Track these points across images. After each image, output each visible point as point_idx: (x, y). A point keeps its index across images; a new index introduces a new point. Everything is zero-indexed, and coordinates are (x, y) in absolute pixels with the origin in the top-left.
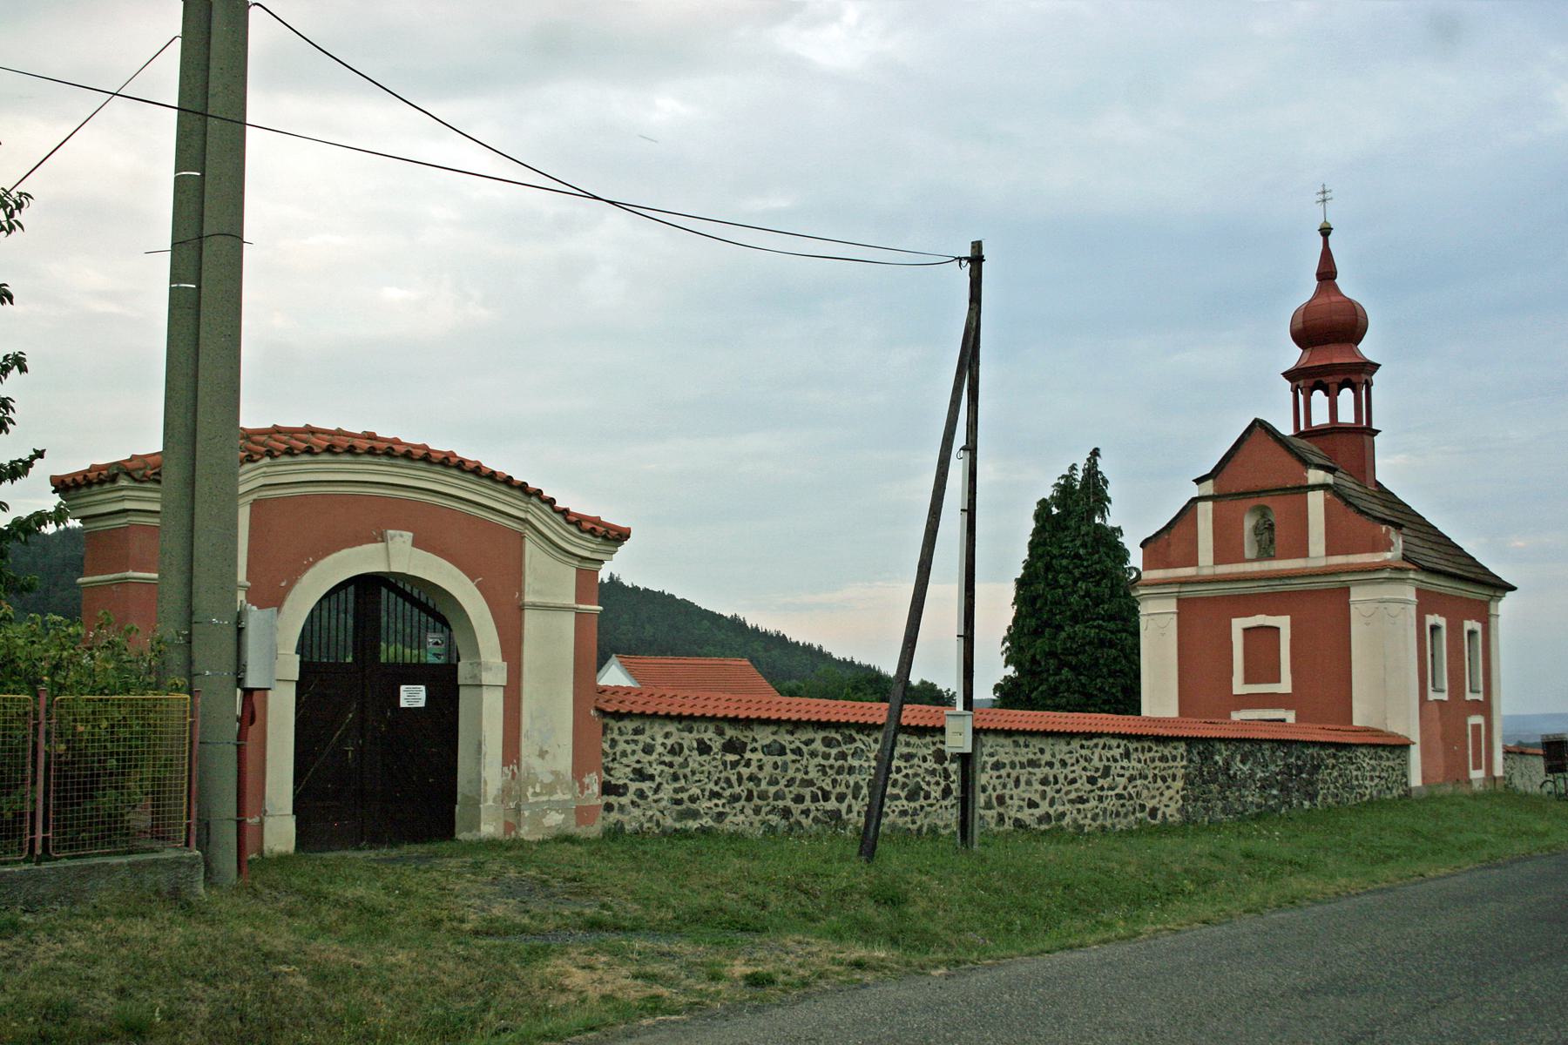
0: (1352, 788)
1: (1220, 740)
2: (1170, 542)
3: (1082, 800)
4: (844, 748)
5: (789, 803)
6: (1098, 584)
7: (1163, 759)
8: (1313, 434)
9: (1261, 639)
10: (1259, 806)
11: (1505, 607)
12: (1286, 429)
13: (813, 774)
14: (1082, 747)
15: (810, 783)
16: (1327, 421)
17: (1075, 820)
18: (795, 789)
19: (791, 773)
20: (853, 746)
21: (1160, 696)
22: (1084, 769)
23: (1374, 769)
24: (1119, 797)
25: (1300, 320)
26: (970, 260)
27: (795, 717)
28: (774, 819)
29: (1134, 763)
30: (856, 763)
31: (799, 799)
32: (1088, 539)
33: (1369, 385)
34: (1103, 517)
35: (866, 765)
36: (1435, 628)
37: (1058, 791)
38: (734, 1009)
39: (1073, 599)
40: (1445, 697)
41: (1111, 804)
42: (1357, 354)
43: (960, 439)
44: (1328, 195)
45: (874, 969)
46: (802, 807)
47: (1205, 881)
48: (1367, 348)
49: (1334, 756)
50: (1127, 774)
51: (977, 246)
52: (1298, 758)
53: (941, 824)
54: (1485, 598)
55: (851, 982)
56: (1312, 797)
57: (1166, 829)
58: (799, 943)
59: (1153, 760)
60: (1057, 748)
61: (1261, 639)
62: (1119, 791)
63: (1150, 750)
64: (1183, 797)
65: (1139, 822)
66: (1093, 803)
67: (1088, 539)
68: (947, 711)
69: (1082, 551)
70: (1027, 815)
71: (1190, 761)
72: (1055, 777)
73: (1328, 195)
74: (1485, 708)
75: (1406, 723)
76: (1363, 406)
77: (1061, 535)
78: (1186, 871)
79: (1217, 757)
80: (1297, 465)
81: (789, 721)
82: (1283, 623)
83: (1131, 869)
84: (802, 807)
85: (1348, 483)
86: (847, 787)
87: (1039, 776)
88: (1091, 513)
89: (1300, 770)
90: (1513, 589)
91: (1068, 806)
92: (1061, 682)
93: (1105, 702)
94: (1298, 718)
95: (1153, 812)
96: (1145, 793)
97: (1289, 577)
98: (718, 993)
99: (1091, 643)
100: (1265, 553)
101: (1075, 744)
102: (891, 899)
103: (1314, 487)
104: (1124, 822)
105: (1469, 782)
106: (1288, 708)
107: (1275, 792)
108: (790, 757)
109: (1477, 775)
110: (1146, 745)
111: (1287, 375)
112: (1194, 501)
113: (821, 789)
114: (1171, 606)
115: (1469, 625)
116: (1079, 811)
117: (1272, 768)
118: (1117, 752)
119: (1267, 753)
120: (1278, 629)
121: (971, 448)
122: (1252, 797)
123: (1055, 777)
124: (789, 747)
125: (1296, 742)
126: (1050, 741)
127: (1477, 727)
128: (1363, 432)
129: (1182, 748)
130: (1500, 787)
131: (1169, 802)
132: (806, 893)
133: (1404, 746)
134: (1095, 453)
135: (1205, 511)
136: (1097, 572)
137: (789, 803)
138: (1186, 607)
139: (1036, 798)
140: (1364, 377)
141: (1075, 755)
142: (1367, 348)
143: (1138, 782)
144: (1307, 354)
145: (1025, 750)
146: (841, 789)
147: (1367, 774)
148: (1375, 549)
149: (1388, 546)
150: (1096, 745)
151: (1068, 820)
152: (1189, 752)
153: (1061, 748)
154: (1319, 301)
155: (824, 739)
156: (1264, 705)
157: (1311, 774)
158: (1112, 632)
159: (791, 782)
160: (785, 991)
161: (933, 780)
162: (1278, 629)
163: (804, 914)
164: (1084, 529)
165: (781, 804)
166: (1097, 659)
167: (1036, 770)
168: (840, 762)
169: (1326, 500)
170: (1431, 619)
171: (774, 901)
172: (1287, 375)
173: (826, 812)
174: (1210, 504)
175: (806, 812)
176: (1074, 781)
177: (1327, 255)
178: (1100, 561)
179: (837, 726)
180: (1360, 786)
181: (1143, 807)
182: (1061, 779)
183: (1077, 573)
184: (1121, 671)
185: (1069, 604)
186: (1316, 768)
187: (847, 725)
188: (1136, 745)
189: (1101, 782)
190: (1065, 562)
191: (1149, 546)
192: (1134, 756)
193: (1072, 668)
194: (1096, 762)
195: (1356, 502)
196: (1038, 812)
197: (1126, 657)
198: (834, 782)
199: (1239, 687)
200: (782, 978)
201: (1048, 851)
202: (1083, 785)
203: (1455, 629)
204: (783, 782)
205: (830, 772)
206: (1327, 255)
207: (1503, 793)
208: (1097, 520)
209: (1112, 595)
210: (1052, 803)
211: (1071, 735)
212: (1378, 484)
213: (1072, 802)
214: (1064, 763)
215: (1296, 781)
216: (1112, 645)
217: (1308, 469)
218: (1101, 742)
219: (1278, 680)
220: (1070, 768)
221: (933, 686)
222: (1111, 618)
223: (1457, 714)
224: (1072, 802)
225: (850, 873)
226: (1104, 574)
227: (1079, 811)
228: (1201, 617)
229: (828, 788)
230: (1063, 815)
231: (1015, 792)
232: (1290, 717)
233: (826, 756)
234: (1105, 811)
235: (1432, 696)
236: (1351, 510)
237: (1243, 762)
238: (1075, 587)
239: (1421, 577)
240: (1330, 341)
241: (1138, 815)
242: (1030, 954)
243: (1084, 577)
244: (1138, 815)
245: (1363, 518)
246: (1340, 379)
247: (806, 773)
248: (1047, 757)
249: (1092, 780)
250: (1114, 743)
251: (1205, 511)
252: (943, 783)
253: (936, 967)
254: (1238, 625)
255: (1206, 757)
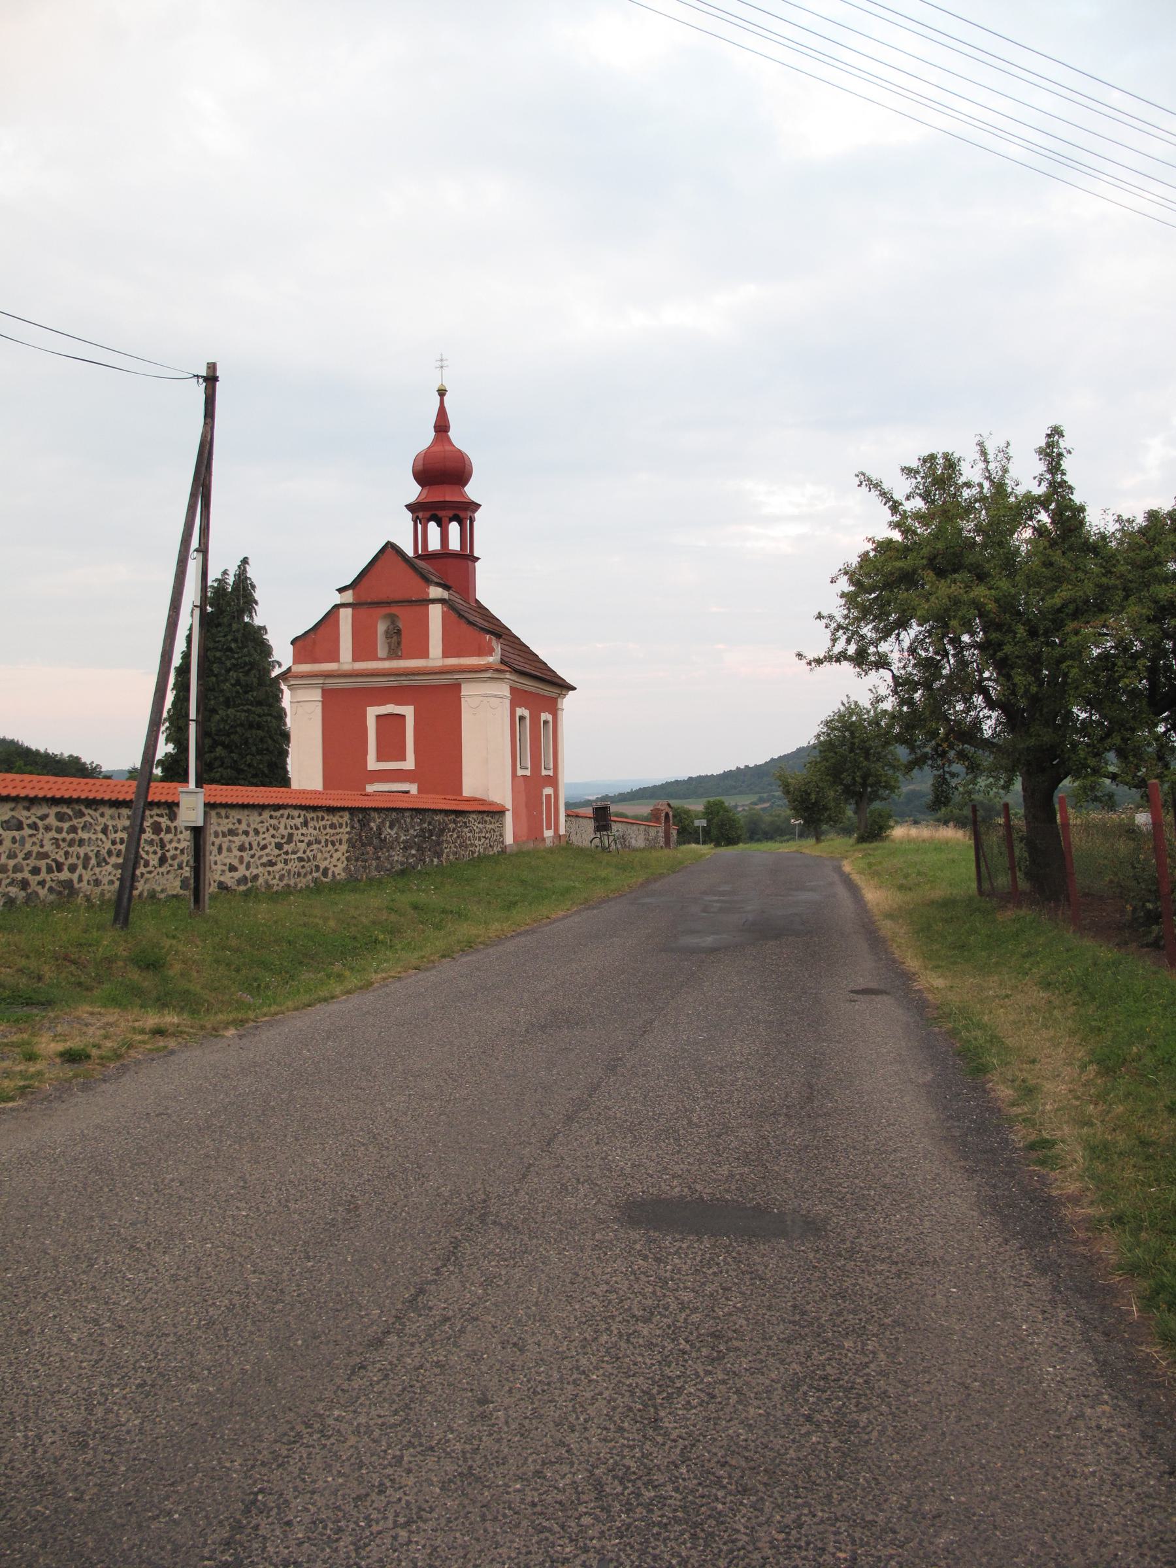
0: (466, 847)
1: (376, 809)
2: (314, 642)
3: (271, 864)
4: (75, 822)
5: (26, 875)
6: (247, 673)
7: (333, 826)
8: (428, 556)
9: (391, 726)
10: (402, 863)
11: (568, 703)
12: (410, 553)
13: (48, 847)
14: (271, 817)
15: (45, 856)
16: (439, 548)
17: (266, 882)
18: (32, 862)
19: (28, 847)
20: (82, 820)
21: (305, 767)
22: (273, 836)
23: (481, 831)
24: (301, 859)
25: (421, 463)
26: (206, 379)
27: (32, 794)
28: (13, 891)
29: (311, 830)
30: (85, 836)
31: (36, 871)
32: (239, 635)
33: (472, 521)
34: (251, 617)
35: (94, 837)
36: (522, 718)
37: (253, 856)
38: (63, 1089)
39: (226, 686)
40: (528, 773)
41: (294, 866)
42: (463, 495)
43: (195, 543)
44: (445, 363)
45: (173, 1035)
46: (38, 878)
47: (394, 931)
48: (472, 491)
49: (455, 822)
50: (306, 840)
51: (212, 367)
52: (430, 823)
53: (159, 889)
54: (555, 695)
55: (158, 1050)
56: (439, 855)
57: (336, 887)
58: (92, 1014)
59: (325, 828)
60: (251, 818)
61: (391, 726)
62: (300, 854)
63: (323, 818)
64: (348, 859)
65: (315, 880)
66: (280, 866)
67: (239, 635)
68: (181, 788)
69: (233, 645)
70: (229, 879)
71: (353, 827)
72: (250, 844)
73: (445, 363)
74: (553, 781)
75: (501, 793)
76: (467, 537)
77: (214, 630)
78: (374, 923)
79: (372, 824)
80: (416, 580)
81: (26, 798)
82: (408, 711)
83: (332, 923)
84: (38, 878)
85: (457, 599)
86: (78, 858)
87: (238, 844)
88: (241, 612)
89: (431, 833)
90: (574, 689)
91: (261, 869)
92: (216, 759)
93: (255, 776)
94: (419, 791)
95: (326, 870)
96: (319, 856)
97: (414, 674)
98: (40, 1073)
99: (242, 725)
100: (393, 654)
101: (266, 814)
102: (151, 964)
103: (434, 601)
104: (304, 880)
105: (544, 839)
106: (412, 782)
107: (413, 852)
108: (27, 831)
109: (548, 834)
110: (320, 814)
111: (478, 559)
112: (337, 607)
113: (55, 860)
114: (317, 695)
115: (545, 716)
116: (269, 873)
117: (411, 832)
118: (298, 821)
119: (408, 820)
120: (404, 716)
121: (203, 550)
122: (397, 856)
123: (250, 844)
124: (26, 822)
125: (429, 810)
126: (246, 812)
127: (548, 796)
128: (467, 557)
129: (346, 816)
130: (563, 843)
131: (336, 862)
132: (74, 962)
133: (499, 813)
134: (245, 561)
135: (346, 615)
136: (245, 664)
137: (26, 875)
138: (330, 698)
139: (236, 863)
140: (469, 514)
141: (266, 824)
142: (472, 491)
143: (315, 846)
144: (425, 492)
145: (226, 821)
146: (72, 860)
147: (475, 833)
148: (480, 653)
149: (490, 652)
150: (282, 816)
151: (261, 881)
152: (352, 820)
153: (254, 818)
154: (435, 449)
155: (57, 814)
156: (392, 778)
157: (439, 836)
158: (259, 716)
159: (28, 856)
160: (103, 1065)
161: (151, 850)
162: (404, 716)
163: (80, 984)
164: (235, 626)
165: (19, 876)
166: (247, 739)
167: (235, 838)
168: (72, 836)
169: (443, 612)
170: (520, 711)
171: (48, 972)
172: (410, 507)
173: (60, 882)
174: (349, 611)
175: (42, 883)
176: (264, 847)
177: (442, 413)
178: (250, 655)
179: (68, 802)
180: (472, 845)
181: (317, 867)
182: (255, 846)
183: (228, 664)
184: (267, 749)
185: (222, 691)
186: (442, 831)
187: (78, 801)
188: (313, 815)
189: (286, 847)
190: (218, 654)
191: (299, 643)
192: (311, 824)
193: (225, 746)
194: (282, 831)
195: (466, 615)
196: (237, 875)
197: (271, 737)
198: (67, 853)
199: (373, 764)
200: (94, 1052)
201: (263, 911)
202: (272, 850)
203: (535, 719)
204: (21, 856)
205: (63, 844)
206: (442, 413)
207: (565, 846)
208: (247, 620)
209: (260, 684)
210: (248, 867)
211: (262, 808)
212: (477, 601)
213: (264, 865)
214: (257, 832)
215: (421, 845)
216: (259, 727)
217: (422, 585)
218: (286, 812)
219: (403, 758)
220: (262, 836)
221: (78, 759)
222: (259, 703)
223: (536, 783)
224: (264, 865)
225: (110, 942)
226: (252, 665)
227: (269, 873)
228: (342, 706)
229: (61, 860)
230: (256, 877)
231: (218, 858)
232: (413, 789)
233: (59, 830)
234: (289, 872)
235: (520, 772)
236: (463, 621)
237: (391, 827)
238: (224, 680)
239: (513, 678)
240: (443, 483)
241: (315, 875)
242: (296, 1009)
243: (235, 667)
244: (315, 875)
245: (471, 628)
246: (451, 513)
247: (42, 846)
248: (243, 827)
249: (279, 846)
250: (296, 813)
251: (346, 615)
252: (160, 852)
253: (226, 1028)
254: (372, 712)
255: (364, 824)
